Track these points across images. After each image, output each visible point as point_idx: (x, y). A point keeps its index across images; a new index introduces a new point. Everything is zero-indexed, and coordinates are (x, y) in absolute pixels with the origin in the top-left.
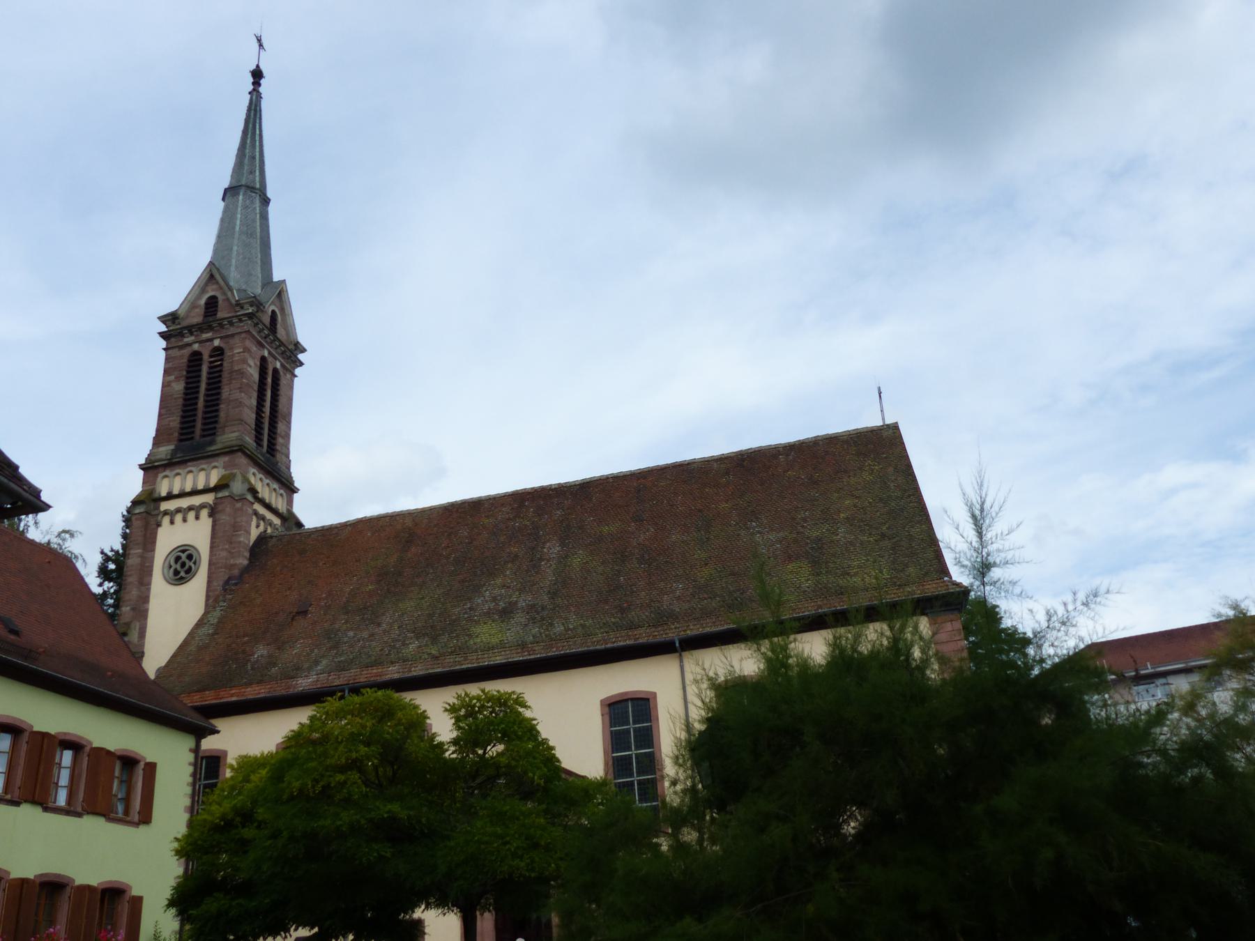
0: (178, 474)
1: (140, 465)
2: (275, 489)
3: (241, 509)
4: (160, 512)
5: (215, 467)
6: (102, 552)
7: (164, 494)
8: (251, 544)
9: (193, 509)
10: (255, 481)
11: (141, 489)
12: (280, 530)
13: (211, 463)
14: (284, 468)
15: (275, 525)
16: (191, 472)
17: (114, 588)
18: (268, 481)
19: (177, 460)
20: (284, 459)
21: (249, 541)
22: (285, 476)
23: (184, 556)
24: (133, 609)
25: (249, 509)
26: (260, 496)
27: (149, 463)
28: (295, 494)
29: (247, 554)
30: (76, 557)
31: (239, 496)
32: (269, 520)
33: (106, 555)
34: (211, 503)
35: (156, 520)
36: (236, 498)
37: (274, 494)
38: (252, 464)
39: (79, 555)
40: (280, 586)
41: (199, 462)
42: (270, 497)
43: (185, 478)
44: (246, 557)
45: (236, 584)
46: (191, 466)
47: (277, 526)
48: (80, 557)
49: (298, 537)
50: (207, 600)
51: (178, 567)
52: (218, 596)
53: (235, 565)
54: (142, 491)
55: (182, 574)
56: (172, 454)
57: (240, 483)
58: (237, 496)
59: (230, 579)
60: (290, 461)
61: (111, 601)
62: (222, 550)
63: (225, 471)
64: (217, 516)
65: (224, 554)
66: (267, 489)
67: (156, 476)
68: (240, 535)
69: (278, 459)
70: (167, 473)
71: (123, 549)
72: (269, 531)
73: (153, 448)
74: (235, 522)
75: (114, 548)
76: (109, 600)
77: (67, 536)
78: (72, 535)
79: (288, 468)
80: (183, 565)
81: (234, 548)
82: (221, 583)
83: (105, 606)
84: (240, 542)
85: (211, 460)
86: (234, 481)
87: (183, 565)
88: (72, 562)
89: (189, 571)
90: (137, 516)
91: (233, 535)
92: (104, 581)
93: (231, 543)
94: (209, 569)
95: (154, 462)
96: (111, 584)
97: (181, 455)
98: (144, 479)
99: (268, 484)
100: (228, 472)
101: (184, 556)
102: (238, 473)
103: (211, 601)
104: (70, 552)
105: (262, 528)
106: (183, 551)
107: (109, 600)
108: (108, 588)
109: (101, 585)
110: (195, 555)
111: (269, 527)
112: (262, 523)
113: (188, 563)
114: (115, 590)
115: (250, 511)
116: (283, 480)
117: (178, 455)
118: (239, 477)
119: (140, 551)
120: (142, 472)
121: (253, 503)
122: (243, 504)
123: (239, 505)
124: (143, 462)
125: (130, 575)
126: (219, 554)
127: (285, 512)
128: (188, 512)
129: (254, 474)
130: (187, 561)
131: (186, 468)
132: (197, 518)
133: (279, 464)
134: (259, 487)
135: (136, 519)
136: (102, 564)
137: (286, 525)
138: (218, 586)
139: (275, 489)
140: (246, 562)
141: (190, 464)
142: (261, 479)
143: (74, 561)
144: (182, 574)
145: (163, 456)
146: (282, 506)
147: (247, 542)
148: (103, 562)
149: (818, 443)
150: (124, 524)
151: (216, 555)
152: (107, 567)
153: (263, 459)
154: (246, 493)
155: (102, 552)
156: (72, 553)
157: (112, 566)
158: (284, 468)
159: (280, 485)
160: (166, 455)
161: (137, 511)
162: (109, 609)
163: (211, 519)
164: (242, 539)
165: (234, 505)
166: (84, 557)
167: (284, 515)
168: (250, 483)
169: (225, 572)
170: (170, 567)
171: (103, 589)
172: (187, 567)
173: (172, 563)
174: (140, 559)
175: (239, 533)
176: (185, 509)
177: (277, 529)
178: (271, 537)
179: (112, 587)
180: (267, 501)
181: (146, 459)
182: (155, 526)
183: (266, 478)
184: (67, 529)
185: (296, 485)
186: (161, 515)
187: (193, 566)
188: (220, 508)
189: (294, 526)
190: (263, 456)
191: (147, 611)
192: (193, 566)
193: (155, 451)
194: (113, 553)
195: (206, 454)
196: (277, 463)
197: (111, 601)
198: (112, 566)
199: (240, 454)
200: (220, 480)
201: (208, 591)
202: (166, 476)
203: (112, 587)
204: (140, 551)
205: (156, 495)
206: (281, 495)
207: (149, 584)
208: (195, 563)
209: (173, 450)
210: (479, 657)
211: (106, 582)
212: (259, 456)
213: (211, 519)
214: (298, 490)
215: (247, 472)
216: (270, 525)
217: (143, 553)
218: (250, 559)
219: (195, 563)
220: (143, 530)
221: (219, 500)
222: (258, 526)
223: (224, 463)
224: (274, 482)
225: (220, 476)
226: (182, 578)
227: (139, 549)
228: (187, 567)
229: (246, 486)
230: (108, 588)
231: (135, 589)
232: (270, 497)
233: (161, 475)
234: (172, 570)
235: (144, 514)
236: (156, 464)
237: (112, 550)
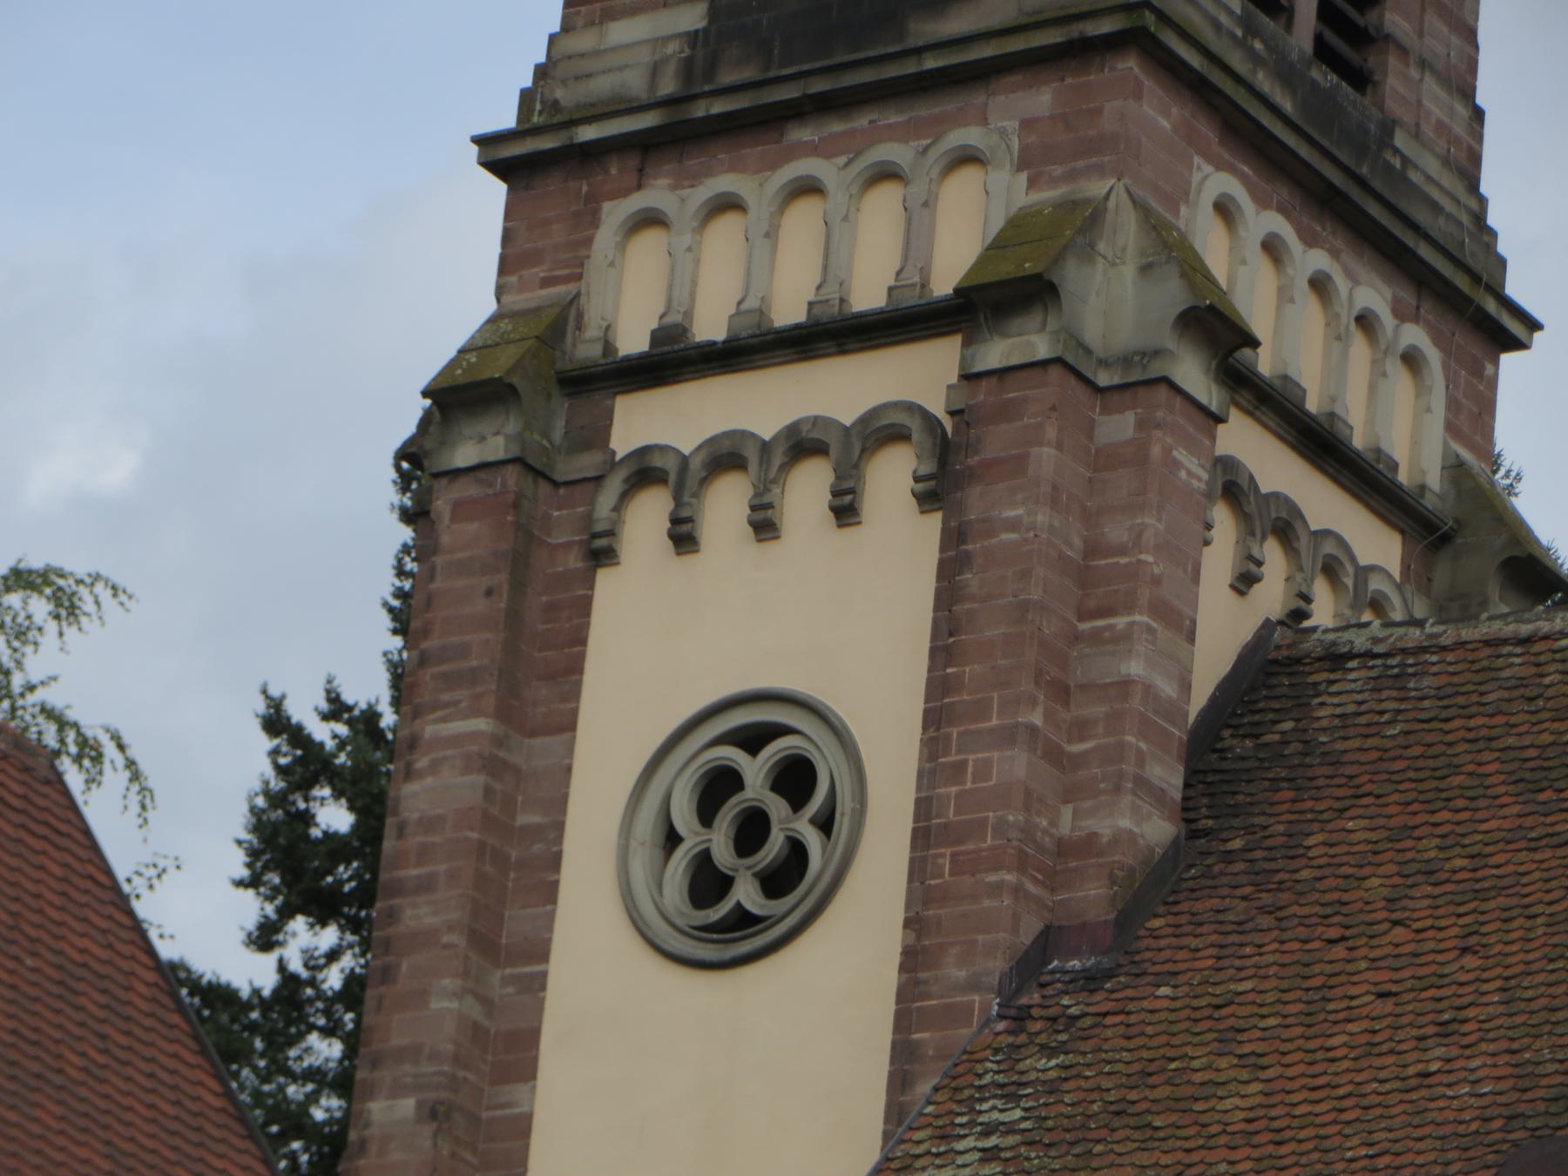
0: (728, 204)
1: (481, 141)
2: (1365, 321)
3: (1134, 456)
4: (612, 464)
5: (967, 158)
6: (276, 722)
7: (633, 341)
8: (1199, 699)
9: (819, 449)
10: (1237, 258)
11: (490, 306)
12: (1397, 615)
13: (935, 127)
14: (1432, 166)
15: (1364, 572)
16: (809, 188)
17: (347, 961)
18: (1318, 260)
19: (719, 107)
20: (1435, 99)
21: (1186, 687)
22: (1438, 227)
23: (755, 770)
24: (433, 1113)
25: (1180, 454)
26: (1265, 363)
27: (537, 131)
28: (1508, 360)
29: (1170, 777)
30: (89, 752)
31: (1126, 361)
32: (1326, 533)
33: (297, 736)
34: (938, 408)
35: (589, 518)
36: (1103, 379)
37: (1360, 348)
38: (1207, 131)
39: (105, 739)
40: (1388, 1006)
41: (862, 121)
42: (1336, 371)
43: (772, 234)
44: (1158, 796)
45: (1090, 981)
46: (814, 150)
47: (1376, 584)
48: (110, 750)
49: (1516, 665)
50: (900, 1081)
51: (720, 842)
52: (971, 1056)
53: (1086, 846)
54: (493, 320)
55: (746, 894)
56: (687, 70)
57: (1129, 271)
58: (1104, 363)
59: (1049, 942)
60: (1478, 115)
61: (325, 1050)
62: (1007, 737)
63: (1032, 183)
64: (977, 502)
65: (1016, 764)
66: (1310, 311)
67: (589, 218)
68: (1124, 638)
69: (1393, 106)
70: (657, 195)
71: (396, 703)
72: (1324, 612)
73: (567, 27)
74: (1093, 550)
75: (348, 697)
76: (313, 1039)
77: (40, 607)
78: (67, 608)
79: (1468, 169)
80: (752, 830)
81: (1080, 729)
82: (996, 966)
83: (293, 1077)
84: (1126, 684)
85: (925, 109)
86: (1088, 253)
87: (752, 830)
88: (58, 781)
89: (779, 881)
90: (467, 489)
91: (1077, 638)
92: (286, 913)
93: (1061, 692)
94: (918, 870)
95: (574, 123)
96: (329, 936)
97: (747, 74)
98: (507, 237)
99: (1320, 285)
100: (1046, 195)
101: (755, 770)
102: (1120, 199)
103: (924, 1088)
104: (48, 712)
105: (1271, 597)
106: (753, 739)
107: (313, 1039)
108: (312, 963)
109: (265, 938)
110: (829, 761)
111: (1321, 591)
112: (1273, 554)
113: (786, 823)
114: (351, 980)
115: (1194, 470)
116: (1425, 251)
117: (727, 78)
118: (1125, 232)
119: (482, 724)
120: (498, 189)
121: (1219, 420)
122: (1141, 425)
123: (1118, 427)
124: (506, 118)
125: (426, 886)
126: (983, 771)
127: (1434, 480)
128: (786, 467)
129: (1225, 209)
130: (777, 807)
131: (773, 166)
132: (845, 511)
133: (1400, 140)
134: (1257, 306)
135: (461, 510)
136: (276, 800)
137: (1442, 574)
138: (973, 985)
139: (1365, 321)
140: (1159, 830)
141: (802, 134)
142: (1272, 248)
143: (74, 778)
144: (746, 894)
145: (634, 82)
146: (1416, 443)
147: (1167, 688)
148: (277, 784)
149: (931, 739)
150: (406, 534)
151: (960, 767)
152: (307, 818)
153: (1288, 106)
154: (1170, 342)
155: (276, 722)
156: (62, 723)
157: (334, 817)
158: (1432, 166)
159: (1408, 297)
160: (655, 70)
161: (465, 455)
162: (313, 1098)
163: (934, 523)
164: (1134, 668)
165: (1090, 429)
166: (133, 752)
167: (1430, 502)
168: (1193, 269)
169: (1017, 890)
170: (672, 839)
171: (282, 967)
172: (775, 845)
173: (684, 816)
174: (480, 779)
175: (1120, 622)
176: (765, 447)
177: (1377, 605)
178: (1336, 659)
179: (333, 955)
180: (1312, 405)
181: (526, 97)
182: (574, 561)
183: (1310, 240)
184: (36, 562)
185: (1517, 288)
186: (613, 486)
187: (812, 839)
188: (996, 441)
189: (1494, 592)
190: (1288, 76)
191: (522, 1128)
192: (812, 839)
193: (584, 41)
194: (342, 729)
195: (910, 67)
196: (1388, 127)
197: (325, 1050)
198: (334, 817)
199: (1130, 65)
200: (997, 247)
201: (904, 1021)
202: (650, 220)
203: (333, 955)
204: (482, 724)
205: (587, 351)
206: (1411, 360)
207: (540, 952)
208: (825, 824)
209: (693, 38)
210: (1404, 1020)
211: (299, 924)
212: (1264, 82)
213: (934, 523)
214: (1534, 325)
215: (1181, 195)
216: (1330, 570)
217: (498, 741)
218: (1187, 810)
219: (825, 824)
220: (502, 578)
221: (983, 394)
222: (1245, 581)
223: (1027, 125)
224: (1361, 270)
225: (998, 223)
226: (743, 921)
227: (476, 712)
228: (775, 845)
229: (1172, 295)
230: (312, 963)
231: (448, 983)
232: (1336, 371)
233: (615, 213)
234: (681, 858)
235: (512, 475)
236: (588, 133)
237: (336, 708)
